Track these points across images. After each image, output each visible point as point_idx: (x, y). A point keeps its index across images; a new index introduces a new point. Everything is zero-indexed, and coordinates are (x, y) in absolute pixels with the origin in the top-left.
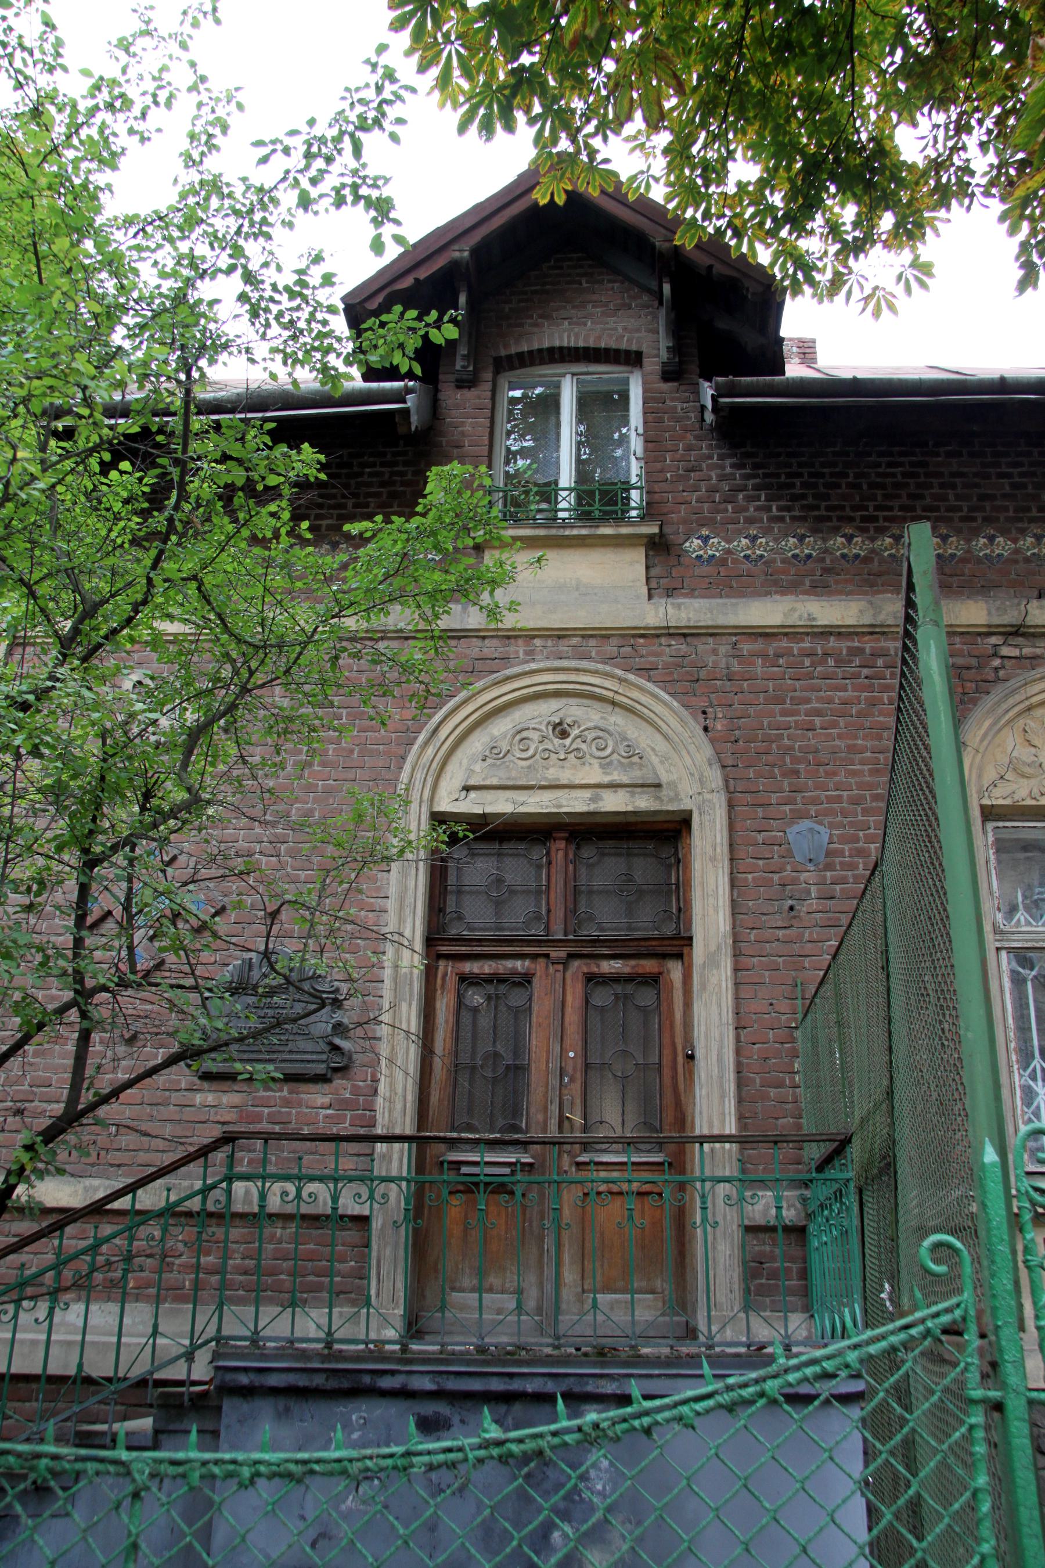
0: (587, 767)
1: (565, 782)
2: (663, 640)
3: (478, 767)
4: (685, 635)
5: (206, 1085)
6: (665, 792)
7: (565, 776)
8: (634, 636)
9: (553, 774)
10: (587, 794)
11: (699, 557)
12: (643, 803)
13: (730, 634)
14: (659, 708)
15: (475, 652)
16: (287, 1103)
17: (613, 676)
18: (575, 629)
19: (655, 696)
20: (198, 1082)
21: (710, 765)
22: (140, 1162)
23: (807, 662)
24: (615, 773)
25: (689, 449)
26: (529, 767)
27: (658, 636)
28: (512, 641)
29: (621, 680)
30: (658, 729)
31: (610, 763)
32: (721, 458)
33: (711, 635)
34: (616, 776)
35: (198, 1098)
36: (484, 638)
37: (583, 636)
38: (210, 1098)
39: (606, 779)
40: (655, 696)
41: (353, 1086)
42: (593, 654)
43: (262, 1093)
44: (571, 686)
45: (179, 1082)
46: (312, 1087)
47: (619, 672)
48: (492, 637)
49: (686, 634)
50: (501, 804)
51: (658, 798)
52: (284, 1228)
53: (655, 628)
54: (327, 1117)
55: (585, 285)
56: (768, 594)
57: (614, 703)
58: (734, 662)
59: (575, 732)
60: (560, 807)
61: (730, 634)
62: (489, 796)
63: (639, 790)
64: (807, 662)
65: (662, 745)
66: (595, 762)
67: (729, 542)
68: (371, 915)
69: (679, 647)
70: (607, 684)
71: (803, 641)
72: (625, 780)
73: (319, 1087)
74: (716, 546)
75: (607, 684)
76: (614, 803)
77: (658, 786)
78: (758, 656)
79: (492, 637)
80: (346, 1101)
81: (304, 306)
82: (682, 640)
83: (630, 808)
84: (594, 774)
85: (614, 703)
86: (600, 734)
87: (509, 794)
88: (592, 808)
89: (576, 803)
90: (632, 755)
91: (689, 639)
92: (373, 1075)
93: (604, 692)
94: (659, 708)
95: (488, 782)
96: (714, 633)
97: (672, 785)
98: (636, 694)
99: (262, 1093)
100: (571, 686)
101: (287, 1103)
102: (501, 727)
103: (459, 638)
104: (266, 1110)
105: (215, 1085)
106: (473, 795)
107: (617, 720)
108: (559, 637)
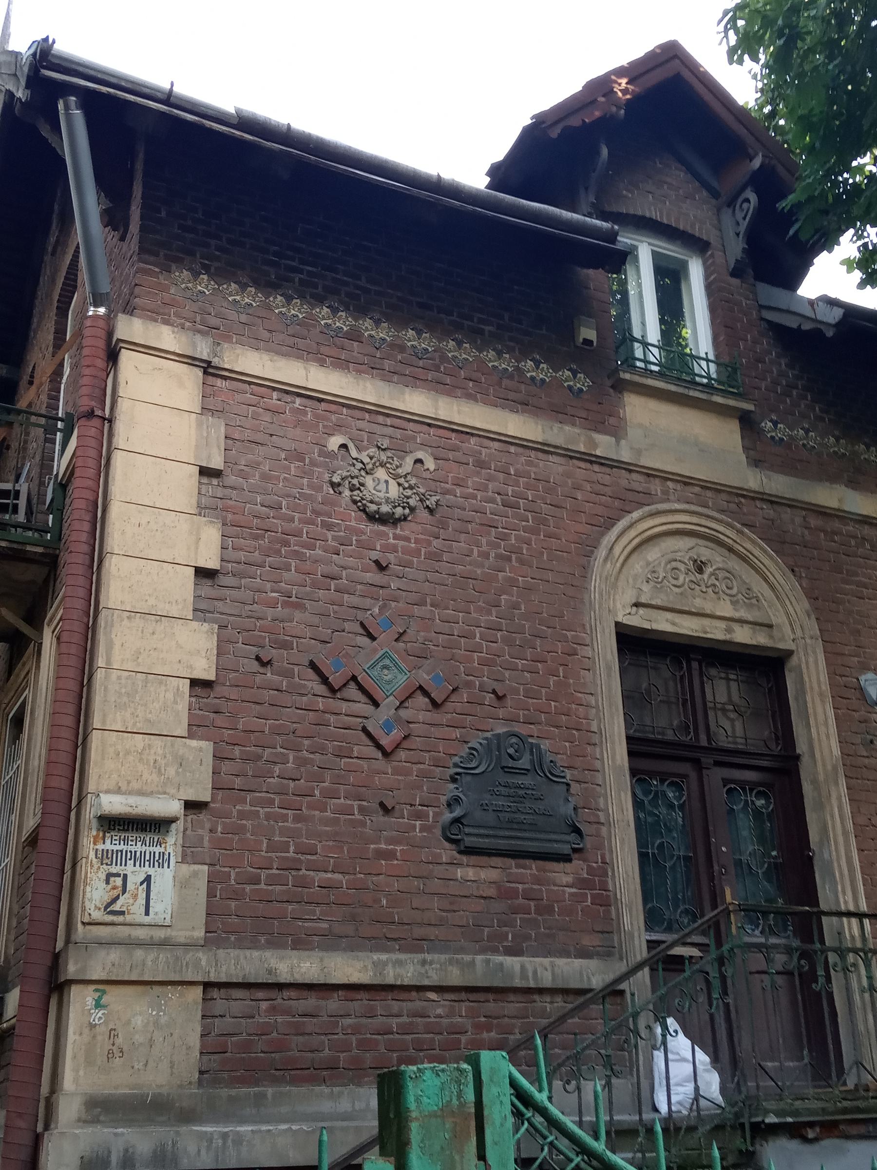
0: (722, 602)
1: (709, 612)
2: (758, 504)
3: (646, 588)
4: (772, 502)
5: (465, 859)
6: (775, 632)
7: (708, 608)
8: (738, 495)
9: (698, 603)
10: (722, 625)
11: (772, 438)
12: (761, 639)
13: (802, 508)
14: (767, 562)
15: (624, 483)
16: (538, 881)
17: (733, 527)
18: (700, 480)
19: (765, 551)
20: (458, 856)
21: (809, 616)
22: (415, 936)
23: (853, 543)
24: (742, 611)
25: (755, 342)
26: (681, 594)
27: (753, 499)
28: (652, 479)
29: (739, 532)
30: (766, 580)
31: (737, 602)
32: (778, 356)
33: (789, 506)
34: (742, 614)
35: (459, 873)
36: (630, 471)
37: (702, 487)
38: (471, 873)
39: (737, 615)
40: (765, 551)
41: (588, 866)
42: (710, 504)
43: (515, 870)
44: (702, 529)
45: (440, 856)
46: (555, 866)
47: (739, 526)
48: (638, 472)
49: (773, 501)
50: (663, 623)
51: (771, 637)
52: (552, 1003)
53: (755, 492)
54: (571, 894)
55: (659, 165)
56: (821, 480)
57: (730, 550)
58: (806, 532)
59: (709, 570)
60: (706, 632)
61: (802, 508)
62: (653, 613)
63: (758, 627)
64: (853, 543)
65: (768, 593)
66: (726, 598)
67: (791, 430)
68: (581, 709)
69: (769, 511)
70: (728, 533)
71: (848, 524)
72: (751, 619)
73: (560, 866)
74: (782, 432)
75: (728, 533)
76: (742, 636)
77: (770, 626)
78: (821, 531)
79: (638, 472)
80: (584, 880)
81: (713, 947)
82: (770, 506)
83: (754, 642)
84: (725, 609)
85: (730, 550)
86: (728, 575)
87: (669, 615)
88: (728, 637)
89: (716, 632)
90: (751, 599)
91: (775, 506)
92: (603, 857)
93: (726, 539)
94: (767, 562)
95: (653, 603)
96: (792, 504)
97: (779, 626)
98: (749, 546)
99: (515, 870)
100: (702, 529)
101: (538, 881)
102: (653, 554)
103: (612, 467)
104: (520, 886)
105: (474, 859)
106: (641, 611)
107: (734, 564)
108: (685, 484)
